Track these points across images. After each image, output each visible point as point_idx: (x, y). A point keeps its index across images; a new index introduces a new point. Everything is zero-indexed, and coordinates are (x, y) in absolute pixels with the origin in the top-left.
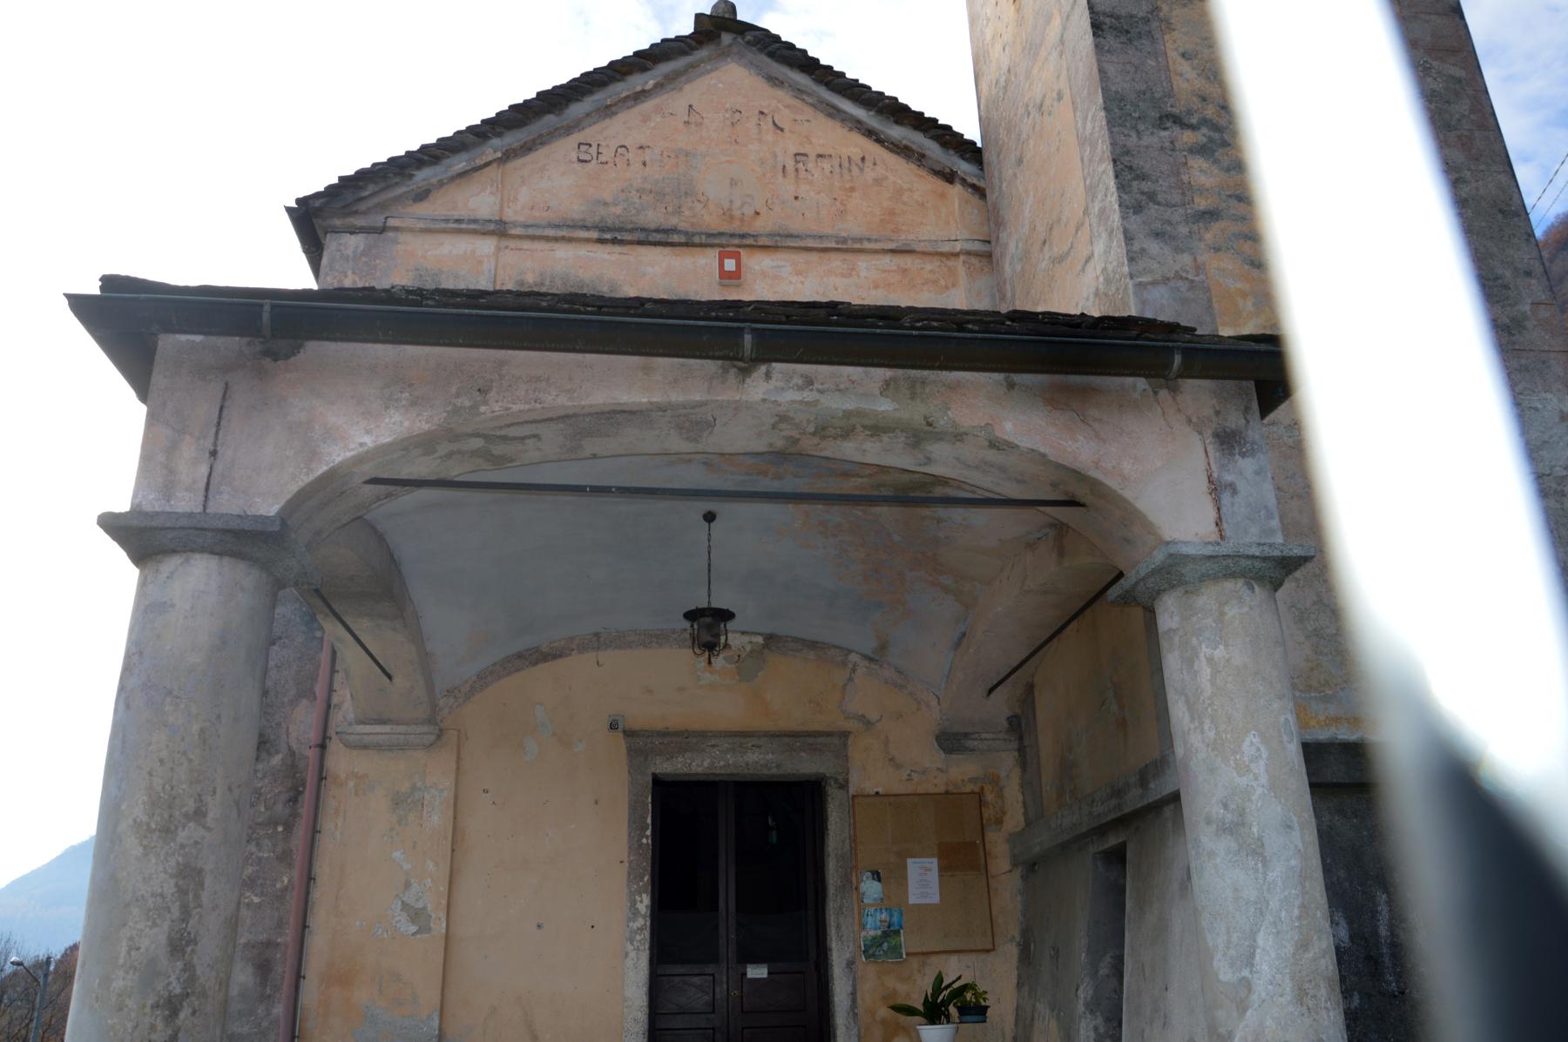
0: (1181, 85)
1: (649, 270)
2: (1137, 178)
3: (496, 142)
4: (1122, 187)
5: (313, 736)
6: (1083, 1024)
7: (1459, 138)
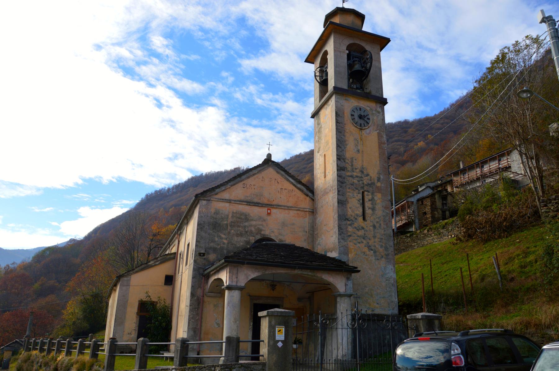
0: (349, 213)
3: (230, 184)
4: (339, 231)
5: (201, 294)
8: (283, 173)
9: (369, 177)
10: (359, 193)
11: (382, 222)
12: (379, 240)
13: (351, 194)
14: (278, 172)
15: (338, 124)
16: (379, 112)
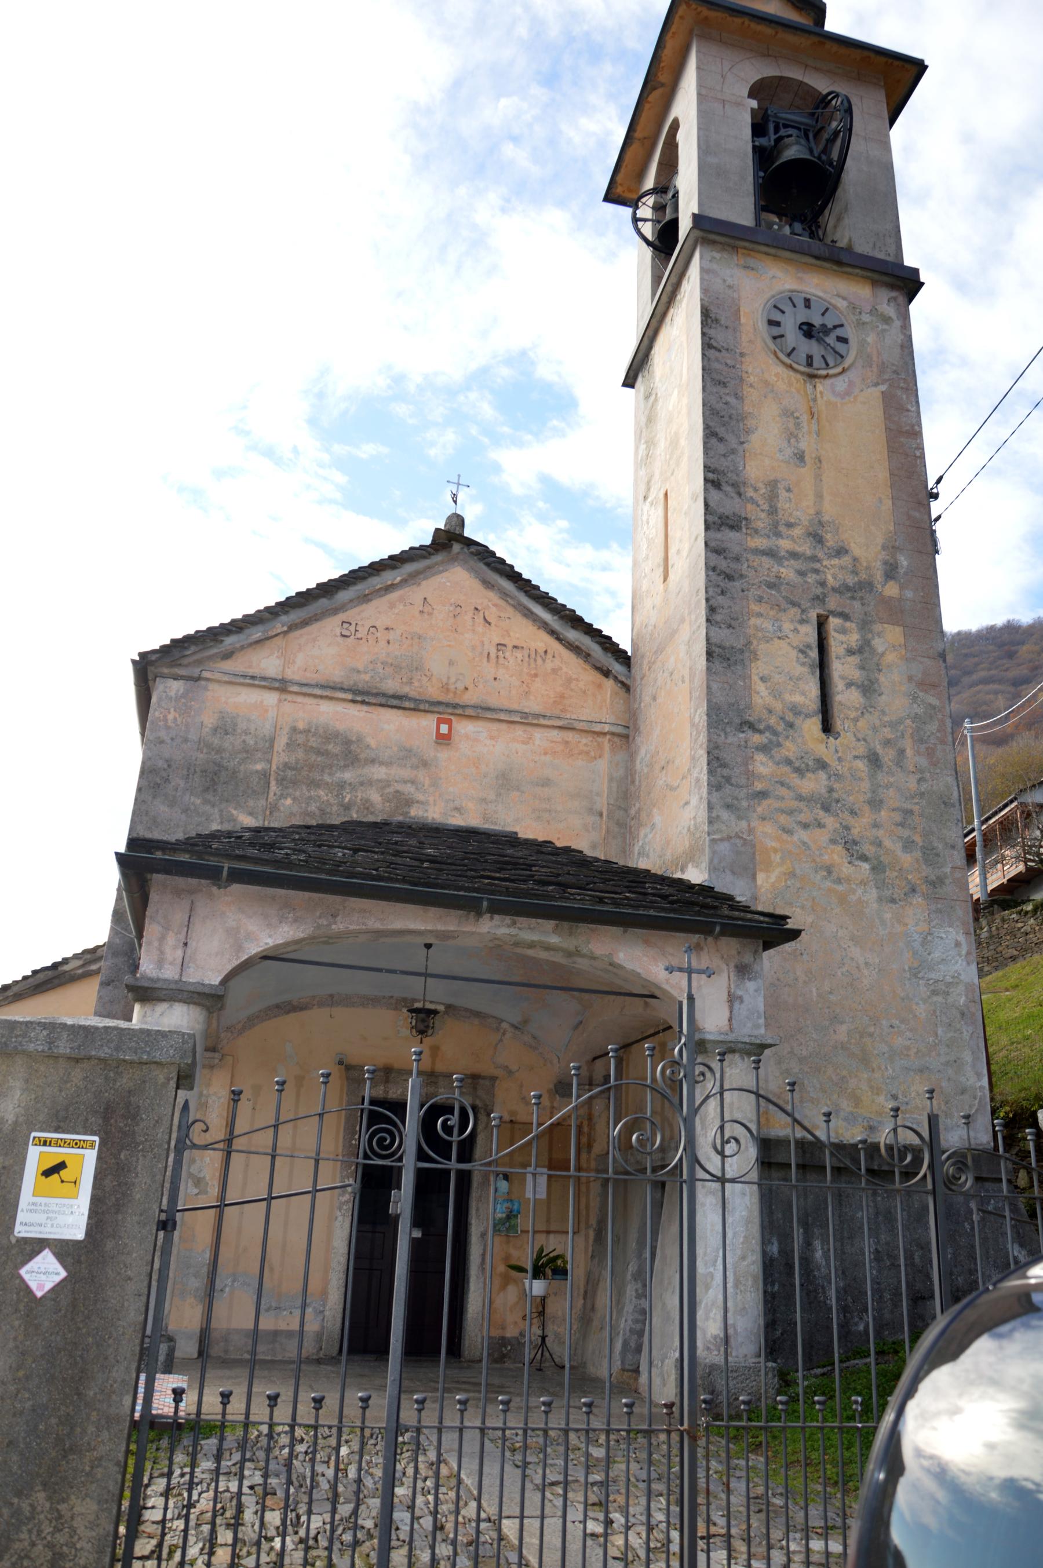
0: (757, 701)
1: (386, 726)
2: (721, 766)
3: (284, 618)
4: (711, 772)
6: (629, 1287)
7: (927, 749)
9: (846, 560)
10: (802, 621)
11: (908, 744)
12: (898, 817)
13: (768, 625)
14: (488, 584)
15: (712, 353)
16: (887, 320)
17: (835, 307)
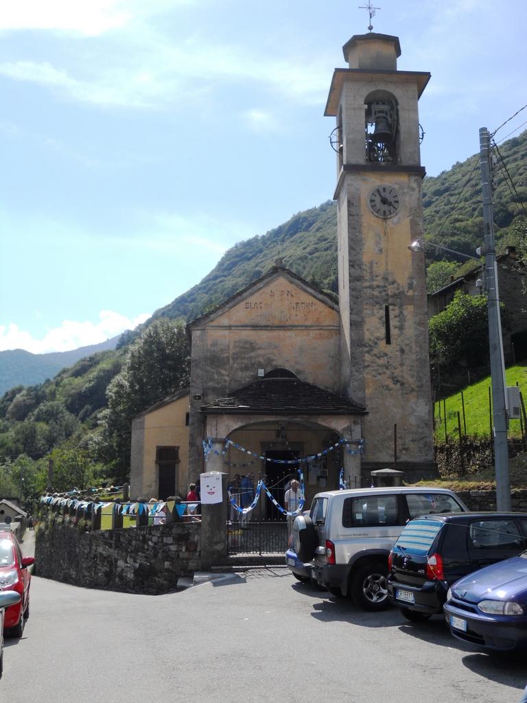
0: (366, 337)
3: (227, 306)
8: (297, 281)
9: (395, 285)
10: (381, 309)
14: (291, 282)
15: (351, 218)
16: (413, 189)
17: (395, 189)
